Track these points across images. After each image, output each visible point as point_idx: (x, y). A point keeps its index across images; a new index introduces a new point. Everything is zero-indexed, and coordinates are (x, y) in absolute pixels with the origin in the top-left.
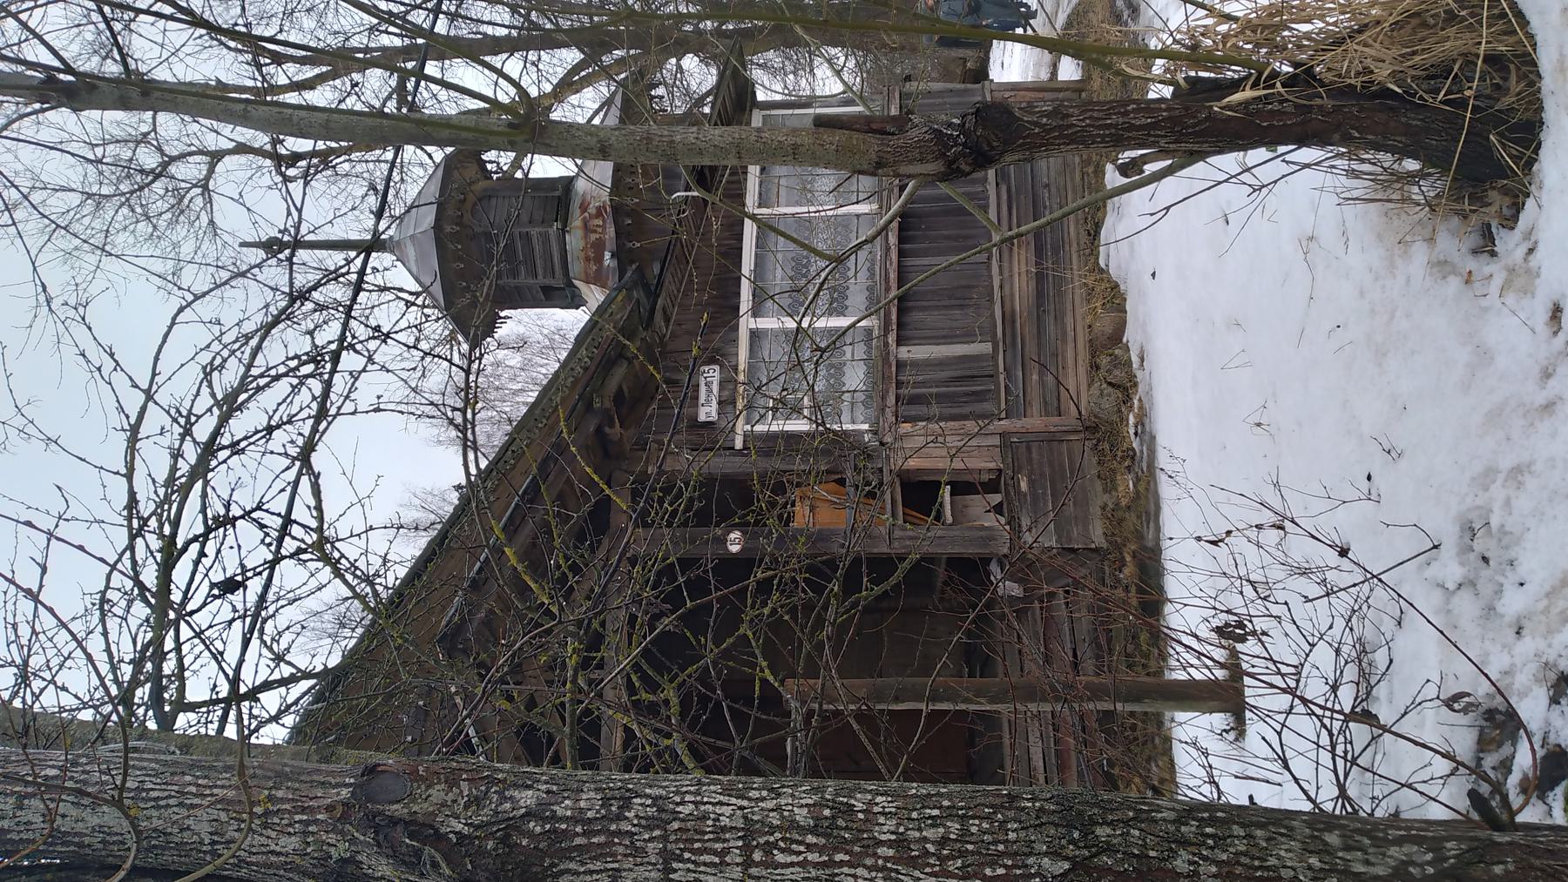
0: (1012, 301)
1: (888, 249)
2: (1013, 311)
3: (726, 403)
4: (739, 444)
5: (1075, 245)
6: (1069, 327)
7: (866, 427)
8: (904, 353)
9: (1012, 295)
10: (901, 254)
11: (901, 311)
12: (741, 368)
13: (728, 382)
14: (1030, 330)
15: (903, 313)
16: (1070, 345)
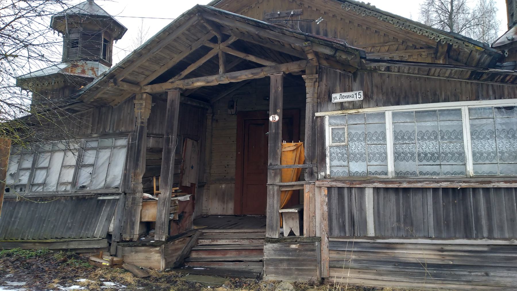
1: (438, 182)
3: (342, 106)
4: (317, 114)
5: (442, 286)
7: (328, 172)
8: (369, 194)
9: (406, 249)
10: (435, 190)
11: (396, 190)
13: (354, 105)
15: (399, 192)
16: (373, 277)
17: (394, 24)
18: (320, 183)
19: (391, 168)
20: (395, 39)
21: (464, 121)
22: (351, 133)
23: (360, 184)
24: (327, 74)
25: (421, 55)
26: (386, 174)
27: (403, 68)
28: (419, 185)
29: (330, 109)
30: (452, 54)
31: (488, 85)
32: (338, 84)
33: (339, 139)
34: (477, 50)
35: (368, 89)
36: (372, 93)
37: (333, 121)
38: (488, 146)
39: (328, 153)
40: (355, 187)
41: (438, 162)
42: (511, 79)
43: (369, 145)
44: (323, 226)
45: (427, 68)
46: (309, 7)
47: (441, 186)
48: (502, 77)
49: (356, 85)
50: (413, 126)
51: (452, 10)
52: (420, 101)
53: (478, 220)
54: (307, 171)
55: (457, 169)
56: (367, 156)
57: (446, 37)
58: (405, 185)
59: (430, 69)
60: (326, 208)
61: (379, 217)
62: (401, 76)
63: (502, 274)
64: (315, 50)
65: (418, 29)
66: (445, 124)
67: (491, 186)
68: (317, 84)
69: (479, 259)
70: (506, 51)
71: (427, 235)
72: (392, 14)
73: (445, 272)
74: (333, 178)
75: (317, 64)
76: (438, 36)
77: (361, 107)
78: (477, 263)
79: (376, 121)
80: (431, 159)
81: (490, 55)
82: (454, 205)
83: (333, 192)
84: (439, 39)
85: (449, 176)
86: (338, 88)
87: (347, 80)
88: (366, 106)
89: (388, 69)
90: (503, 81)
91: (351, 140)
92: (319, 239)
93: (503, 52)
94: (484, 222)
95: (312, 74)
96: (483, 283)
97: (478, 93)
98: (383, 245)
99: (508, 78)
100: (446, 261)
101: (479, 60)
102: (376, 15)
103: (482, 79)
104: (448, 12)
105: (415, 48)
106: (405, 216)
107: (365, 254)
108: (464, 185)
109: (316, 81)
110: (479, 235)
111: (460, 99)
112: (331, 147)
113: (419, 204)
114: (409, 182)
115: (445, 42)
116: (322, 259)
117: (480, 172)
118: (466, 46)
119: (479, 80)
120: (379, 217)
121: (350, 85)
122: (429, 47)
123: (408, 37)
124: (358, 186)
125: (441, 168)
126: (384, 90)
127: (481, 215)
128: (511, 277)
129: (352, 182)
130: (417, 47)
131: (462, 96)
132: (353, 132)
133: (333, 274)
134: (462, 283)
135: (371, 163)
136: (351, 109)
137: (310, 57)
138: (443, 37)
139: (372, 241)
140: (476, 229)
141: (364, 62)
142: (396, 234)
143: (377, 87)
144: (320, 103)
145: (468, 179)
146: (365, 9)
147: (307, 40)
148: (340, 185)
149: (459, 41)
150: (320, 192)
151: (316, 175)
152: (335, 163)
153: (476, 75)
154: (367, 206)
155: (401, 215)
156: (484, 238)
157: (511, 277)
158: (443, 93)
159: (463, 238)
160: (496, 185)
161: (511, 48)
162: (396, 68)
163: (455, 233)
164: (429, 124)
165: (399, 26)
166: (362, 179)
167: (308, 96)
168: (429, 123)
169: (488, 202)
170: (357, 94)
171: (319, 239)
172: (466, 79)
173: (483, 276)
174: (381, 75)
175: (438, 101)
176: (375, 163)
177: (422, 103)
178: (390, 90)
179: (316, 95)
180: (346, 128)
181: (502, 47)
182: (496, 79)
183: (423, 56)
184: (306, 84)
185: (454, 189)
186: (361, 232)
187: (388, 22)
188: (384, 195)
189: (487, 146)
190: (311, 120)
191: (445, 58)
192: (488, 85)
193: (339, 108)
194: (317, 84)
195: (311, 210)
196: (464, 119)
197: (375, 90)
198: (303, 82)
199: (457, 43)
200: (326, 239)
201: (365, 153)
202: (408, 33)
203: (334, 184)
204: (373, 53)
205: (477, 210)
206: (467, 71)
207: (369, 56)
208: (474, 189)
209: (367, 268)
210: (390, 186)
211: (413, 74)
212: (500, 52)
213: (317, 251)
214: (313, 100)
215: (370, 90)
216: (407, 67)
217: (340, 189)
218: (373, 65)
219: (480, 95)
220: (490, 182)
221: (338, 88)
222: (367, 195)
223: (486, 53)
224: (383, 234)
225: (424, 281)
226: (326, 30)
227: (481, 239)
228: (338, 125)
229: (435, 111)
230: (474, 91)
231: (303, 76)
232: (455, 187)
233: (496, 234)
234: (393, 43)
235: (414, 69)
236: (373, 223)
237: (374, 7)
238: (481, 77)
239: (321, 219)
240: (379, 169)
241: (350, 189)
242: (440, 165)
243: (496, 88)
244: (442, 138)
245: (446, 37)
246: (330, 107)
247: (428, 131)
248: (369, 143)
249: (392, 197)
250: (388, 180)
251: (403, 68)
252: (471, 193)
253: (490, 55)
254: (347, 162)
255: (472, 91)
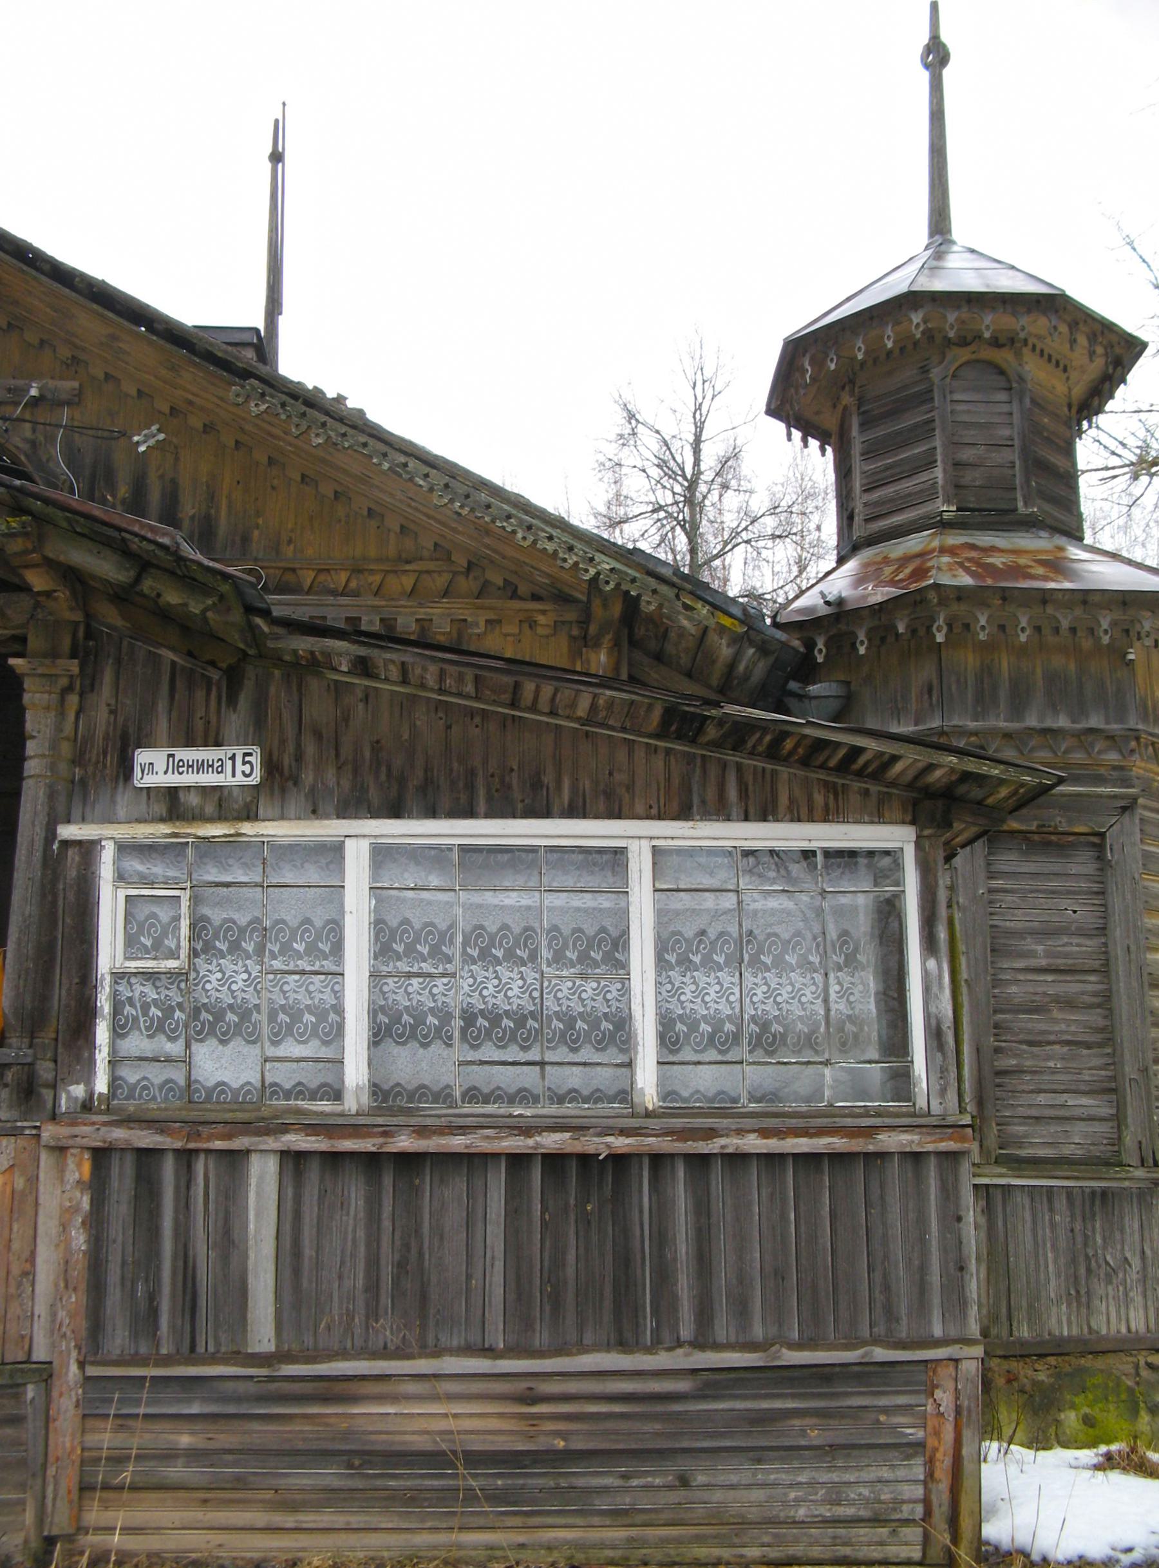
0: (381, 1398)
1: (527, 1131)
2: (354, 1399)
3: (172, 804)
4: (68, 832)
5: (521, 1538)
6: (308, 1519)
7: (101, 1085)
8: (263, 1176)
9: (395, 1399)
10: (518, 1162)
11: (372, 1161)
12: (247, 828)
13: (223, 804)
14: (299, 1433)
15: (380, 1170)
16: (259, 1518)
17: (431, 490)
18: (64, 1131)
19: (356, 1073)
20: (442, 553)
21: (634, 898)
22: (205, 919)
23: (229, 1137)
24: (118, 661)
25: (533, 624)
26: (337, 1095)
27: (418, 671)
28: (457, 1143)
29: (121, 812)
30: (640, 631)
31: (724, 766)
32: (162, 706)
33: (157, 944)
34: (722, 629)
35: (283, 742)
36: (299, 757)
37: (135, 865)
38: (713, 994)
39: (104, 1002)
40: (208, 1151)
41: (534, 1055)
42: (801, 751)
43: (274, 972)
44: (62, 1314)
45: (508, 680)
46: (108, 376)
47: (538, 1145)
48: (768, 738)
49: (235, 721)
50: (450, 905)
51: (697, 474)
52: (482, 806)
53: (664, 1276)
54: (9, 1076)
55: (603, 1078)
56: (264, 1018)
57: (618, 566)
58: (404, 1143)
59: (517, 686)
60: (79, 1240)
61: (297, 1271)
62: (413, 699)
63: (734, 1479)
64: (51, 555)
65: (521, 522)
66: (562, 904)
67: (713, 1146)
68: (73, 700)
69: (658, 1426)
70: (820, 644)
71: (479, 1339)
72: (428, 453)
73: (538, 1480)
74: (119, 1110)
75: (78, 616)
76: (592, 559)
77: (250, 814)
78: (655, 1437)
79: (312, 875)
80: (513, 1039)
81: (764, 649)
82: (584, 1220)
83: (115, 1171)
84: (592, 571)
85: (569, 1109)
86: (162, 726)
87: (200, 694)
88: (270, 814)
89: (363, 667)
90: (773, 753)
91: (205, 950)
92: (46, 1374)
93: (810, 645)
94: (684, 1285)
95: (54, 654)
96: (664, 1516)
97: (690, 791)
98: (308, 1388)
99: (789, 744)
100: (542, 1439)
101: (732, 665)
102: (365, 445)
103: (704, 739)
104: (684, 477)
105: (514, 595)
106: (401, 1266)
107: (236, 1425)
108: (621, 1144)
109: (69, 689)
110: (666, 1335)
111: (625, 810)
112: (118, 976)
113: (454, 1217)
114: (422, 1131)
115: (612, 585)
116: (51, 1459)
117: (685, 1094)
118: (687, 607)
119: (693, 741)
120: (297, 1271)
121: (214, 719)
122: (562, 598)
123: (488, 547)
124: (218, 1144)
125: (543, 1077)
126: (346, 751)
127: (675, 1260)
128: (763, 1485)
129: (194, 1127)
130: (523, 589)
131: (633, 798)
132: (216, 915)
133: (93, 1515)
134: (596, 1520)
135: (281, 1051)
136: (211, 820)
137: (38, 581)
138: (606, 564)
139: (264, 1372)
140: (656, 1311)
141: (266, 629)
142: (359, 1342)
143: (318, 735)
144: (83, 782)
145: (643, 1121)
146: (323, 418)
147: (18, 510)
148: (146, 1139)
149: (664, 589)
150: (61, 1170)
151: (47, 1094)
152: (136, 1044)
153: (681, 724)
154: (252, 1226)
155: (383, 1262)
156: (679, 1344)
157: (763, 1485)
158: (566, 784)
159: (608, 1348)
160: (732, 1143)
161: (833, 631)
162: (391, 667)
163: (581, 1329)
164: (511, 899)
165: (451, 501)
166: (240, 1116)
167: (31, 748)
168: (514, 894)
169: (702, 1207)
170: (239, 760)
171: (46, 1374)
172: (650, 736)
173: (670, 1487)
174: (338, 689)
175: (546, 814)
176: (298, 1051)
177: (489, 815)
178: (367, 754)
179: (66, 749)
180: (185, 897)
181: (808, 626)
182: (750, 744)
183: (540, 631)
184: (26, 698)
185: (585, 1159)
186: (223, 1337)
187: (411, 480)
188: (322, 1180)
189: (712, 991)
190: (38, 855)
191: (616, 644)
192: (724, 766)
193: (160, 809)
194: (73, 700)
195: (16, 1246)
196: (637, 889)
197: (310, 749)
198: (12, 685)
199: (654, 591)
200: (74, 1368)
201: (257, 1007)
202: (488, 533)
203: (119, 1134)
204: (356, 594)
205: (662, 1238)
206: (650, 707)
207: (281, 605)
208: (658, 1160)
209: (240, 1483)
210: (348, 1145)
211: (459, 695)
212: (796, 643)
213: (33, 1425)
214: (53, 767)
215: (291, 748)
216: (433, 668)
217: (147, 1157)
218: (303, 644)
219: (696, 800)
220: (711, 1133)
221: (162, 726)
222: (253, 1181)
223: (751, 643)
224: (309, 1340)
225: (455, 1522)
226: (174, 482)
227: (670, 1349)
228: (151, 884)
229: (533, 850)
230: (676, 782)
231: (12, 661)
232: (591, 1150)
233: (722, 1329)
234: (431, 566)
235: (461, 678)
236: (271, 1297)
237: (361, 413)
238: (700, 730)
239: (56, 1285)
240: (312, 1077)
241: (186, 1157)
242: (542, 1064)
243: (750, 779)
244: (558, 958)
245: (618, 566)
246: (123, 803)
247: (505, 927)
248: (277, 964)
249: (355, 1191)
250: (340, 1121)
251: (418, 671)
252: (646, 1174)
253: (764, 649)
254: (181, 1042)
255: (668, 780)
